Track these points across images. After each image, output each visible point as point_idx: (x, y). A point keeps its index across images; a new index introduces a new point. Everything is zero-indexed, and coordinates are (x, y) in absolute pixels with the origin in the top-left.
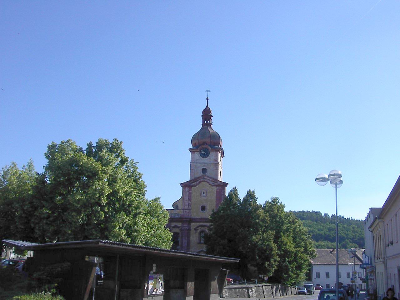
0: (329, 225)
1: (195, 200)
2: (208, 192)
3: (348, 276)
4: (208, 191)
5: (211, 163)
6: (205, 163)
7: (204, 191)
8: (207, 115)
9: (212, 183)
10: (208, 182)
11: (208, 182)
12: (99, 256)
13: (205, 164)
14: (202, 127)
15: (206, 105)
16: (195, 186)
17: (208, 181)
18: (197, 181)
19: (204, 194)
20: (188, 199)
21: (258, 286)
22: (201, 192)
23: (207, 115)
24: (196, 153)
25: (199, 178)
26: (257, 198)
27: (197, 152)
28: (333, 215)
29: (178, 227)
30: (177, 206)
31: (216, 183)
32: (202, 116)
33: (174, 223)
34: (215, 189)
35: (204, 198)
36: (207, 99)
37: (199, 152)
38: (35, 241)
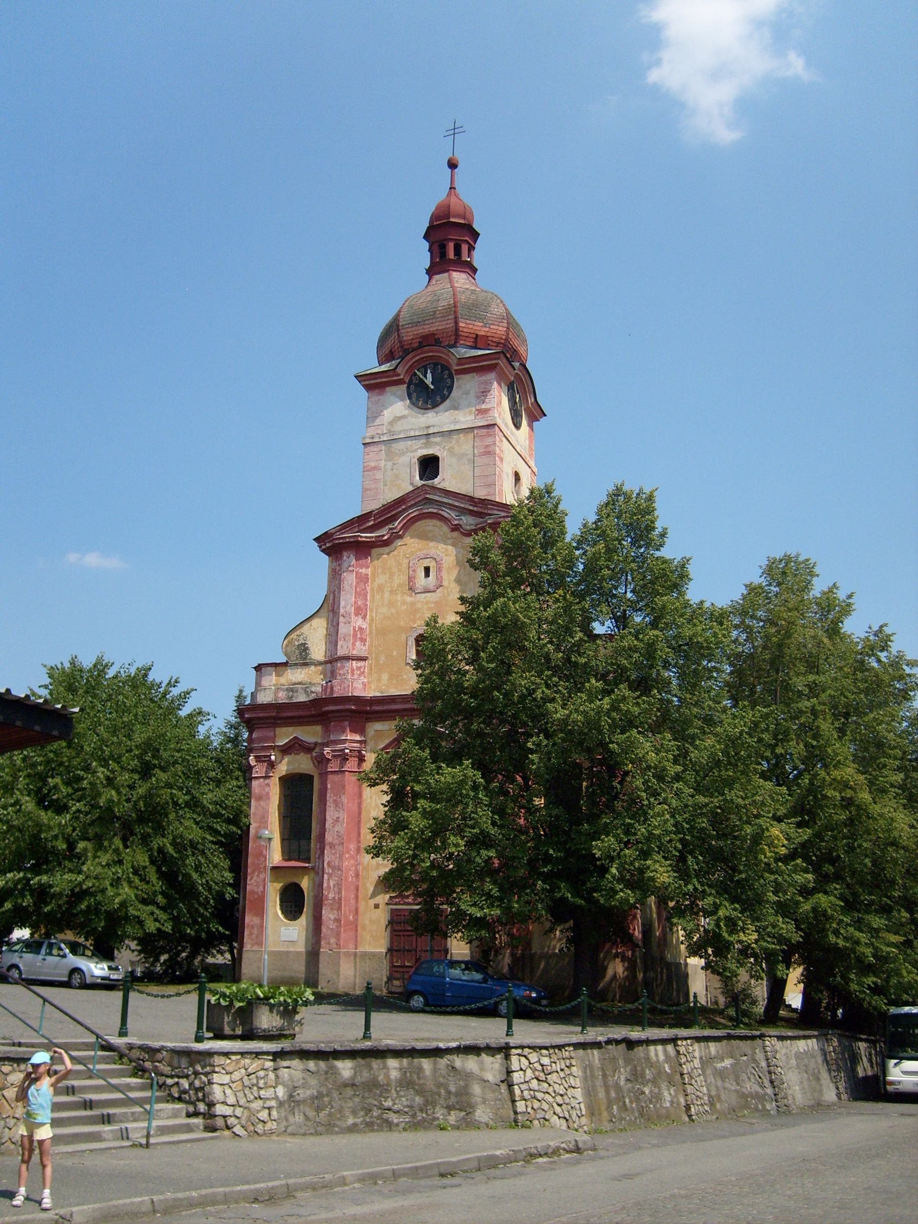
0: (905, 1054)
1: (385, 610)
7: (426, 563)
12: (6, 900)
18: (393, 519)
21: (631, 1044)
24: (394, 394)
26: (663, 535)
27: (393, 388)
29: (307, 749)
33: (291, 729)
36: (453, 165)
38: (286, 911)
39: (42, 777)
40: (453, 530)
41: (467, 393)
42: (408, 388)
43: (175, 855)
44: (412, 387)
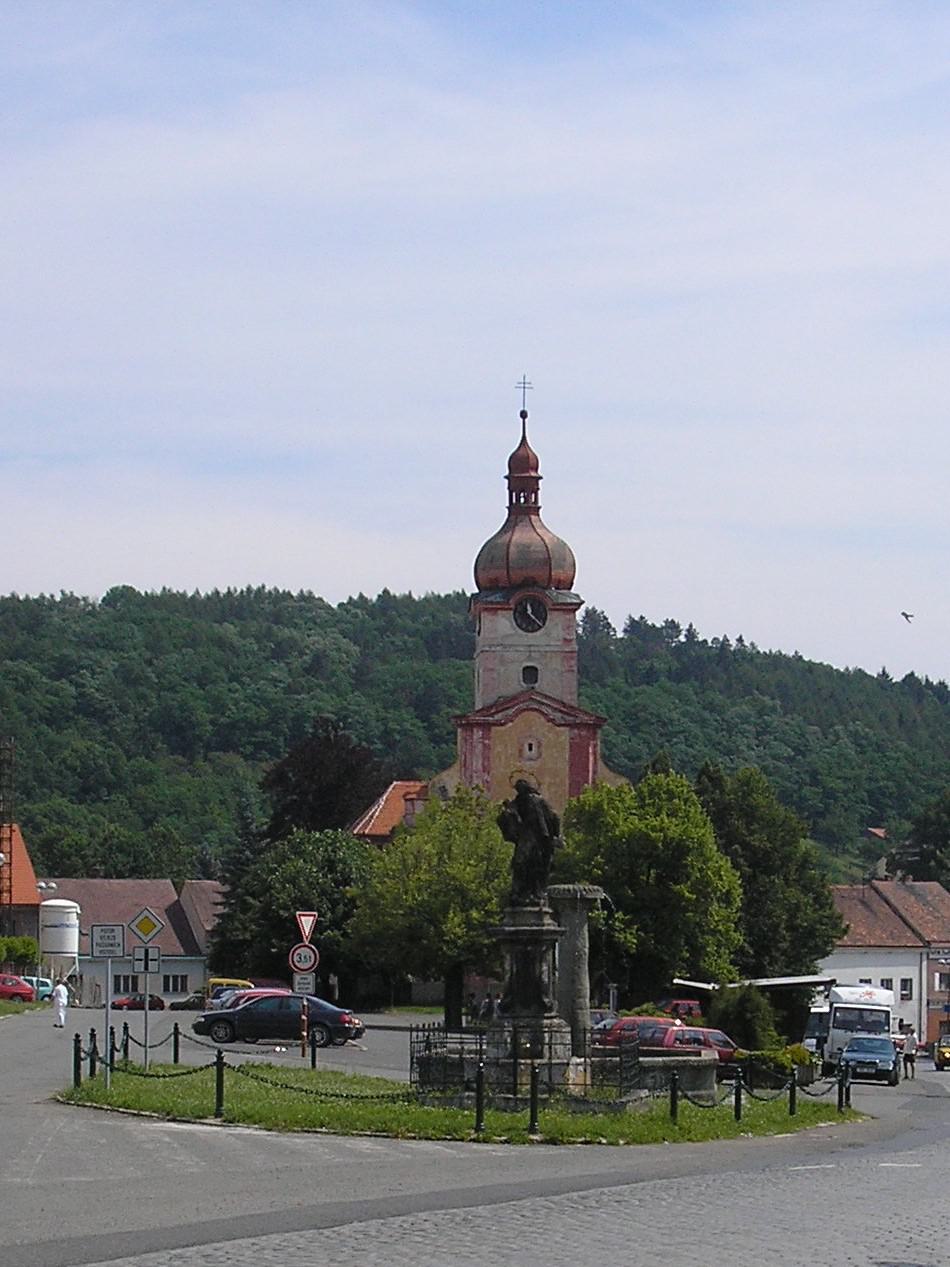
1: (502, 770)
2: (544, 744)
3: (904, 992)
4: (544, 742)
5: (552, 649)
6: (532, 649)
7: (530, 741)
8: (523, 474)
9: (553, 715)
10: (543, 713)
11: (543, 713)
13: (533, 654)
14: (506, 516)
15: (520, 439)
16: (502, 725)
17: (544, 709)
19: (530, 749)
20: (480, 767)
22: (523, 745)
23: (523, 474)
24: (504, 616)
25: (514, 698)
27: (504, 612)
28: (632, 620)
30: (444, 787)
31: (571, 718)
32: (506, 477)
34: (565, 734)
35: (532, 763)
36: (524, 415)
37: (512, 612)
39: (307, 880)
40: (548, 721)
41: (557, 624)
42: (514, 614)
43: (508, 957)
44: (517, 614)
